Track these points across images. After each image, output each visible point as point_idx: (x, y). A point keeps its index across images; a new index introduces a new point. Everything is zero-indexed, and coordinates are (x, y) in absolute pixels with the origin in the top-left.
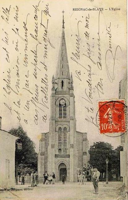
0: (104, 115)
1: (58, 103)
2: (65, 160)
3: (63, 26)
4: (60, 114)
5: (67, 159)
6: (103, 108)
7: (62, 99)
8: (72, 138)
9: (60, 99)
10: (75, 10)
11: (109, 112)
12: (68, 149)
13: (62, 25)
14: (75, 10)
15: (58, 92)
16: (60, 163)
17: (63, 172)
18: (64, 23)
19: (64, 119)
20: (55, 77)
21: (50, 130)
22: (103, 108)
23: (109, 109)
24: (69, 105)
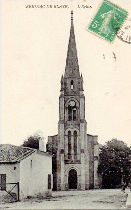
0: (102, 15)
1: (67, 105)
2: (76, 167)
3: (72, 17)
4: (70, 117)
5: (78, 165)
6: (126, 40)
7: (72, 100)
8: (83, 143)
9: (70, 100)
10: (29, 7)
11: (108, 14)
12: (78, 154)
13: (71, 17)
14: (29, 7)
15: (68, 92)
16: (68, 172)
17: (73, 183)
18: (72, 19)
19: (74, 122)
20: (63, 76)
21: (59, 133)
22: (126, 40)
23: (110, 12)
24: (80, 135)
